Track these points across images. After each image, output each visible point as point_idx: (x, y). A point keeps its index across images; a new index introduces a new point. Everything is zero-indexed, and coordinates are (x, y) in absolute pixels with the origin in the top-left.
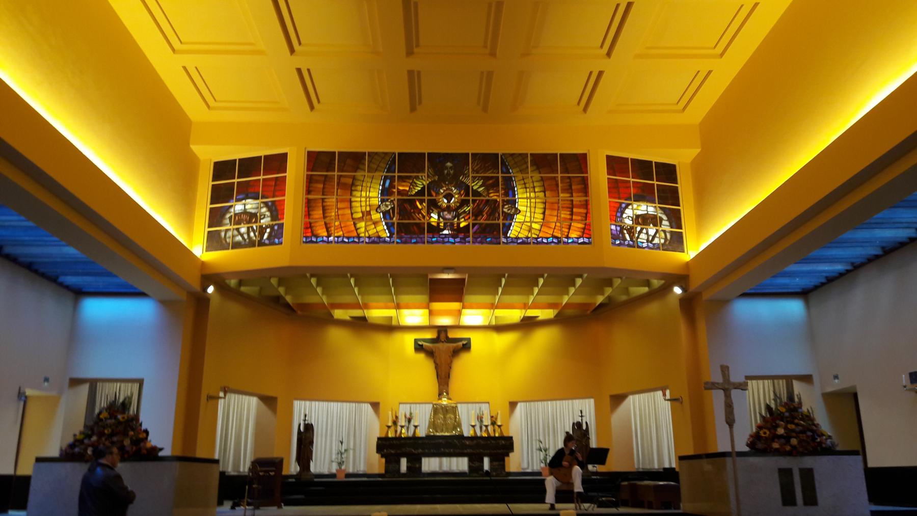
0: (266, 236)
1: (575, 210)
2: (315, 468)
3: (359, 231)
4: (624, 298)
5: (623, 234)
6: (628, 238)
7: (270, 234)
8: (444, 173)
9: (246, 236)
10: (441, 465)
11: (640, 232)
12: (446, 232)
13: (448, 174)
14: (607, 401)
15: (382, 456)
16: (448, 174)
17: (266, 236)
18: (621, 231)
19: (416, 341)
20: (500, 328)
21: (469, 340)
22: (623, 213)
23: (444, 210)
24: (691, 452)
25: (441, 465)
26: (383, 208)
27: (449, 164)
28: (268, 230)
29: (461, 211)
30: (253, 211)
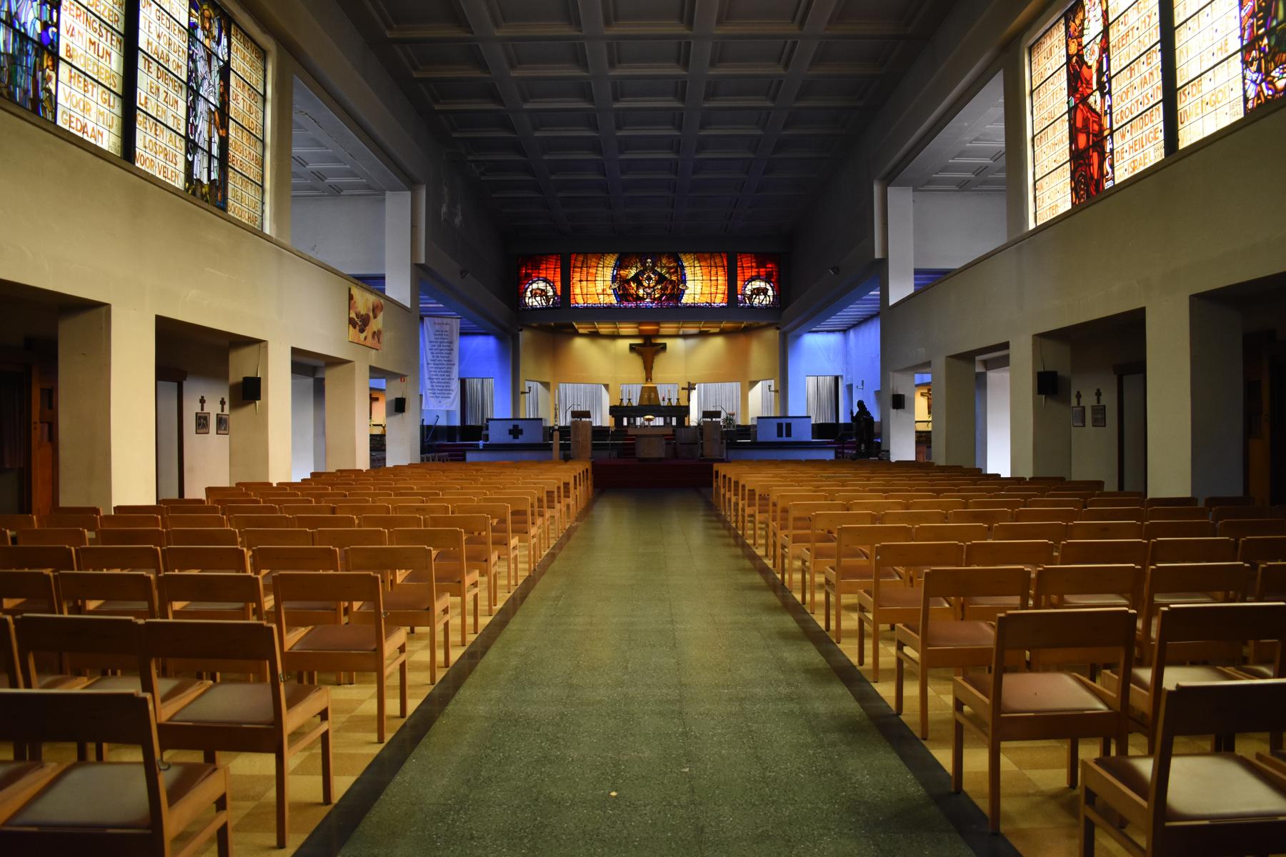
0: (551, 303)
1: (719, 287)
2: (188, 496)
3: (597, 288)
4: (756, 325)
5: (745, 300)
6: (748, 302)
7: (553, 302)
8: (616, 797)
9: (540, 302)
10: (833, 615)
11: (755, 298)
12: (647, 300)
13: (649, 266)
14: (747, 384)
15: (613, 417)
16: (649, 266)
17: (551, 303)
18: (744, 299)
19: (631, 345)
20: (685, 336)
21: (665, 344)
22: (745, 287)
23: (646, 288)
24: (778, 415)
25: (868, 657)
26: (613, 287)
27: (649, 260)
28: (552, 300)
29: (655, 288)
30: (543, 288)
